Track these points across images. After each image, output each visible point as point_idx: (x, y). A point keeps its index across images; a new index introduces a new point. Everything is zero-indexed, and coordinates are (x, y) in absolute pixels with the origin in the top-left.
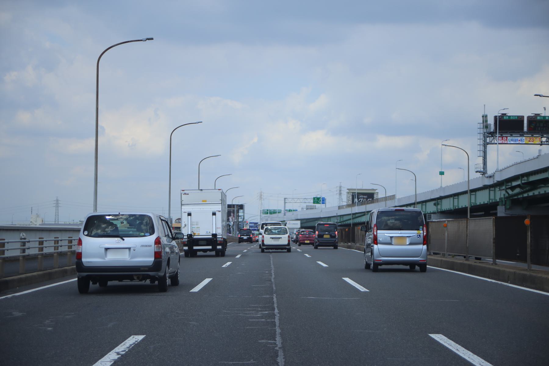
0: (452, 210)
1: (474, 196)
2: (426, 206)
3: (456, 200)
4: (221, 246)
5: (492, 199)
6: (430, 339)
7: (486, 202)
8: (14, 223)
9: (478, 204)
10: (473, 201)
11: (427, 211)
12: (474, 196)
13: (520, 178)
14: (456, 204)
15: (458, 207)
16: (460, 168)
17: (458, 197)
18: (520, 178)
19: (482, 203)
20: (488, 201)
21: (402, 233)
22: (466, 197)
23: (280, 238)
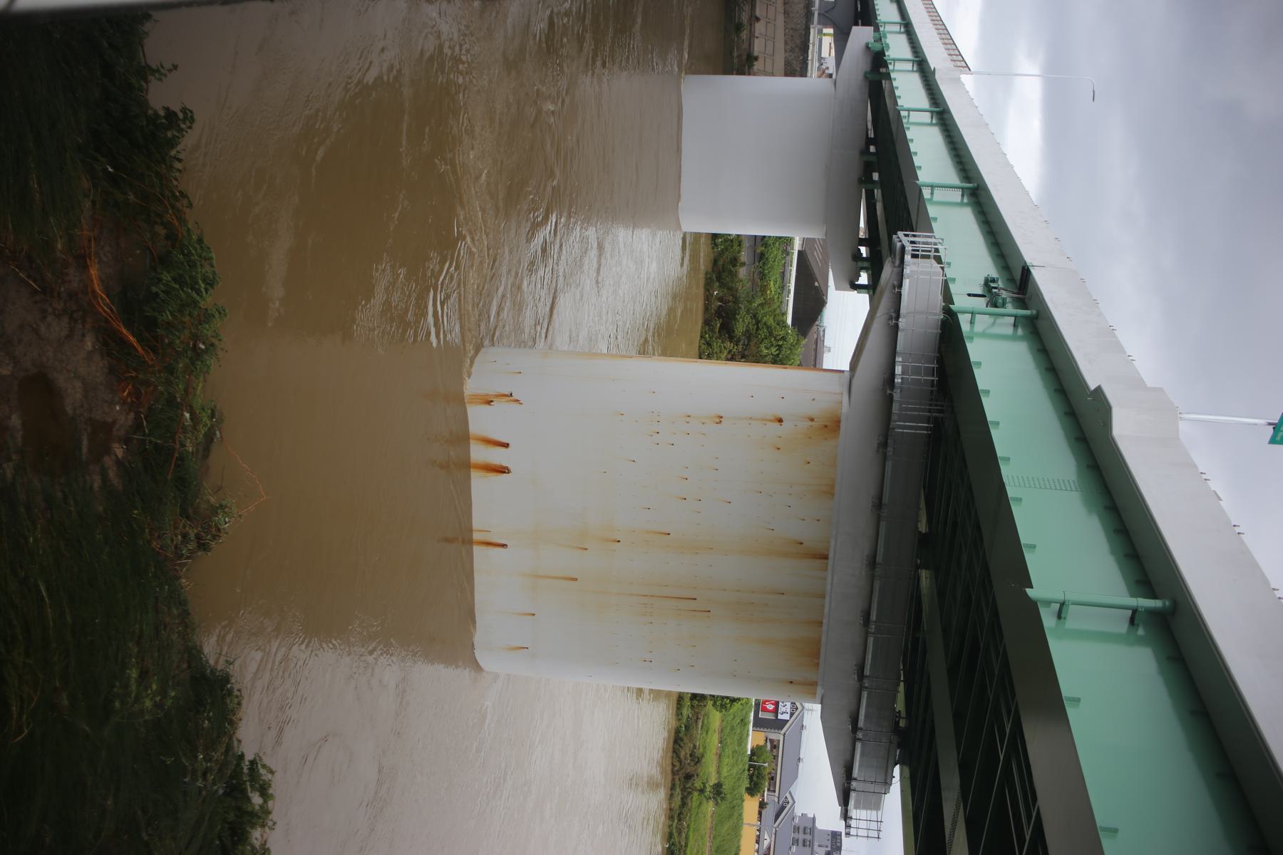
0: (885, 56)
1: (911, 69)
2: (896, 33)
3: (897, 28)
4: (874, 174)
5: (909, 116)
6: (465, 35)
7: (879, 18)
8: (655, 772)
9: (909, 135)
10: (915, 117)
11: (912, 128)
12: (898, 30)
13: (904, 22)
14: (899, 66)
15: (893, 71)
16: (989, 74)
17: (935, 125)
18: (904, 22)
19: (913, 147)
20: (889, 56)
21: (848, 757)
22: (896, 17)
23: (776, 821)
